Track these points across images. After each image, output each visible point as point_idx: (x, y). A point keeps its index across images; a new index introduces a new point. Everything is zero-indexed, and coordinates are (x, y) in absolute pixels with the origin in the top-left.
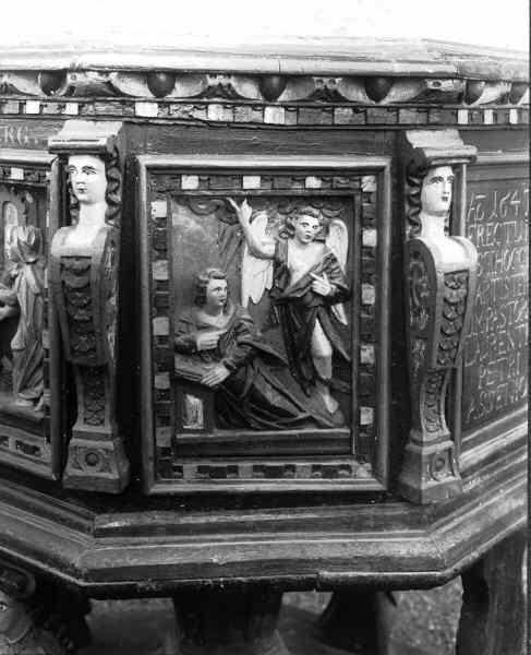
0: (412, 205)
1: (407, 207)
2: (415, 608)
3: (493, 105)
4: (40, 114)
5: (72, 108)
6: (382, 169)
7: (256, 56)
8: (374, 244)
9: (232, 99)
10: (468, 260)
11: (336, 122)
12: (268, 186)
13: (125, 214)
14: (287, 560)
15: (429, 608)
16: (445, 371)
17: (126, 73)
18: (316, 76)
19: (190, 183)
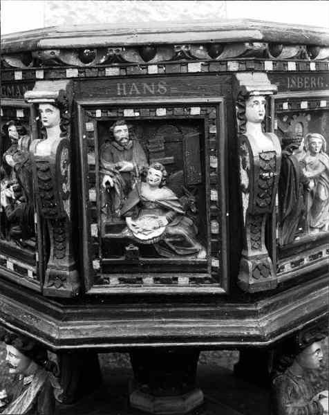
1: (238, 121)
5: (40, 75)
6: (218, 104)
7: (184, 32)
9: (123, 64)
12: (170, 113)
14: (236, 318)
18: (87, 48)
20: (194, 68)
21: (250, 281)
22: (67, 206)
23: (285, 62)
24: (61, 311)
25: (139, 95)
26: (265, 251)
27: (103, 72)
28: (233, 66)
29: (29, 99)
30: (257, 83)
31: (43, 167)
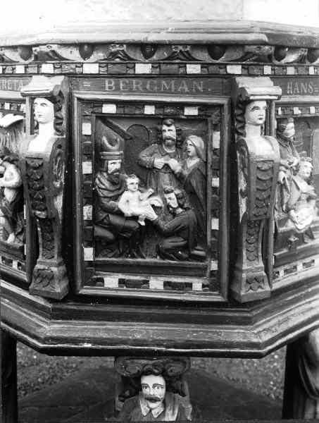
0: (240, 122)
2: (247, 364)
3: (295, 64)
4: (25, 74)
8: (218, 147)
10: (273, 152)
11: (136, 73)
12: (121, 111)
13: (66, 128)
15: (255, 365)
16: (260, 221)
17: (60, 44)
19: (109, 109)
20: (193, 69)
21: (244, 293)
22: (59, 202)
23: (285, 67)
24: (249, 315)
25: (188, 93)
26: (261, 264)
27: (285, 70)
28: (235, 69)
29: (252, 95)
30: (260, 88)
31: (38, 163)
